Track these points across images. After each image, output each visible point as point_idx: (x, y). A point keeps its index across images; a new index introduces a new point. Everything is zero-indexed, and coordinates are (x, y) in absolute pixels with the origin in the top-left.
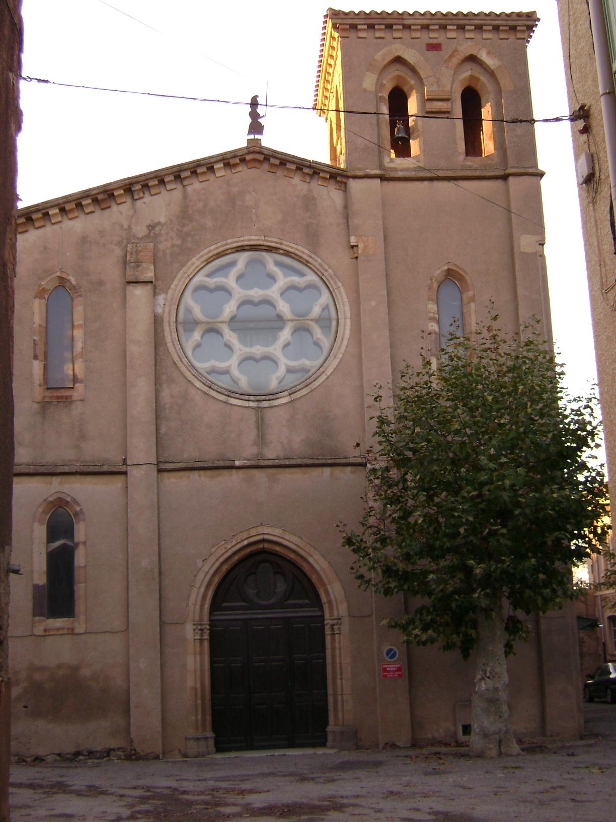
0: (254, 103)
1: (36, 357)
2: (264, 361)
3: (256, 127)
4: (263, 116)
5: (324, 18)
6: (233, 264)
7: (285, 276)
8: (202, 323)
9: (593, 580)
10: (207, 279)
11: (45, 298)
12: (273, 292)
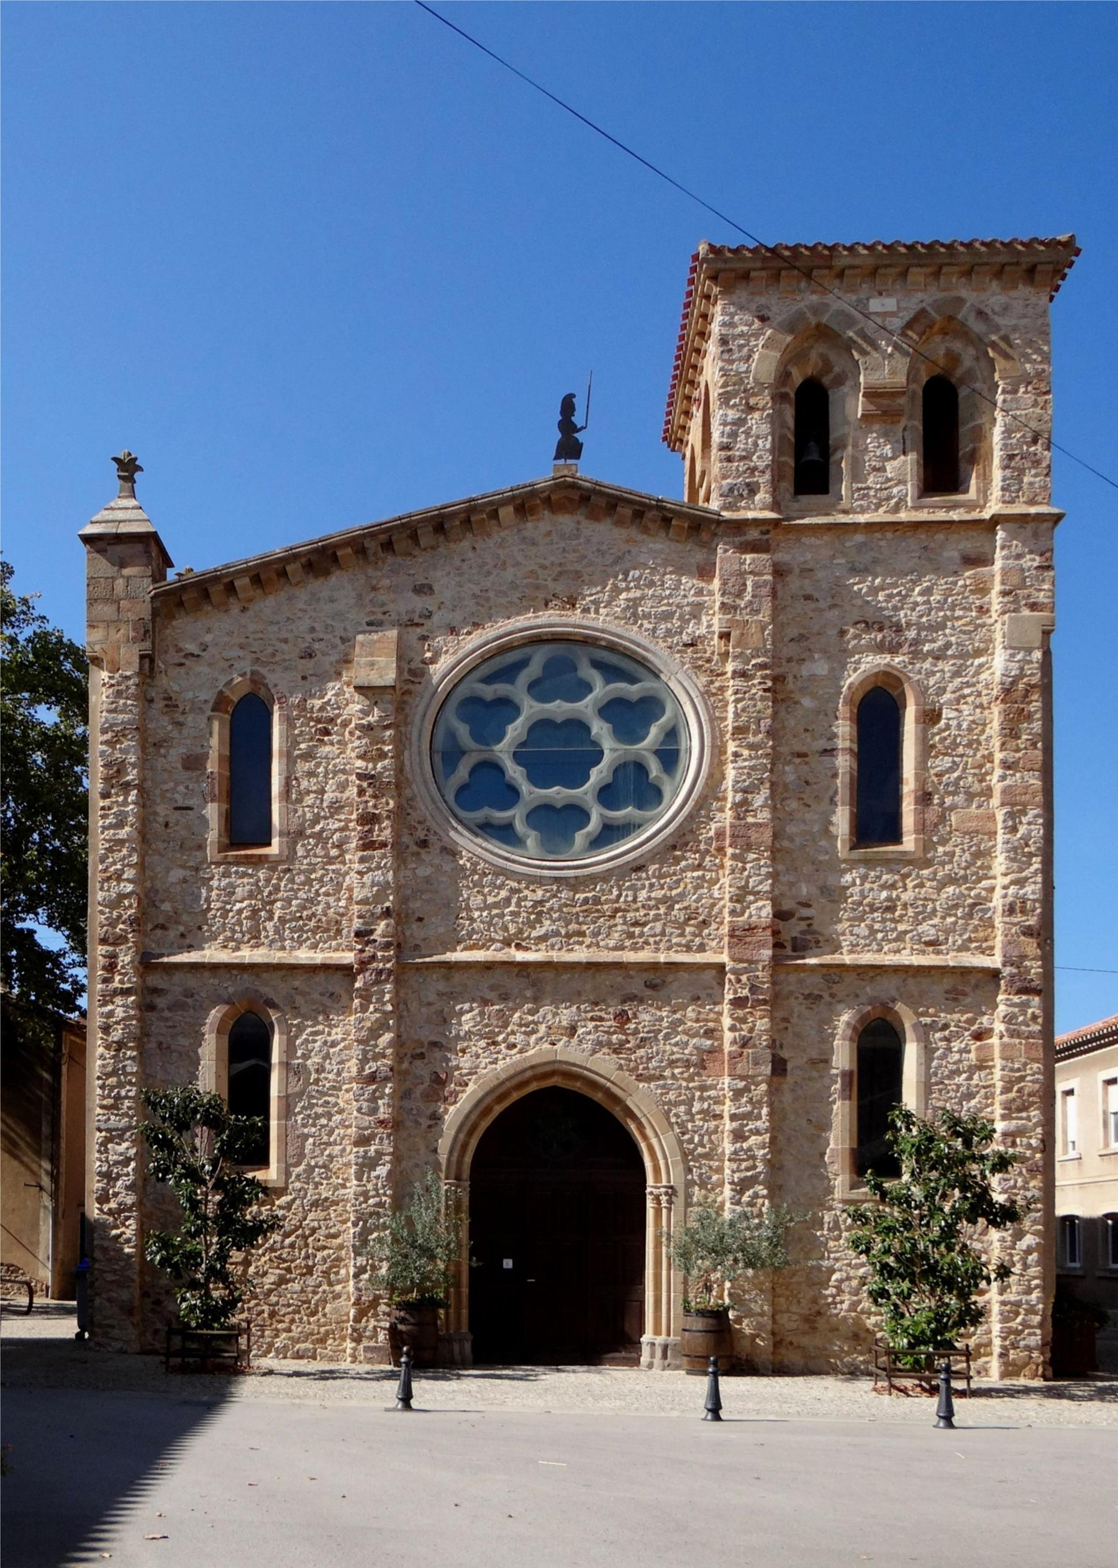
0: (568, 406)
1: (1073, 1143)
2: (566, 521)
3: (569, 448)
4: (583, 428)
5: (677, 360)
6: (523, 664)
7: (608, 682)
8: (473, 751)
9: (285, 826)
10: (482, 686)
11: (227, 712)
12: (586, 707)
